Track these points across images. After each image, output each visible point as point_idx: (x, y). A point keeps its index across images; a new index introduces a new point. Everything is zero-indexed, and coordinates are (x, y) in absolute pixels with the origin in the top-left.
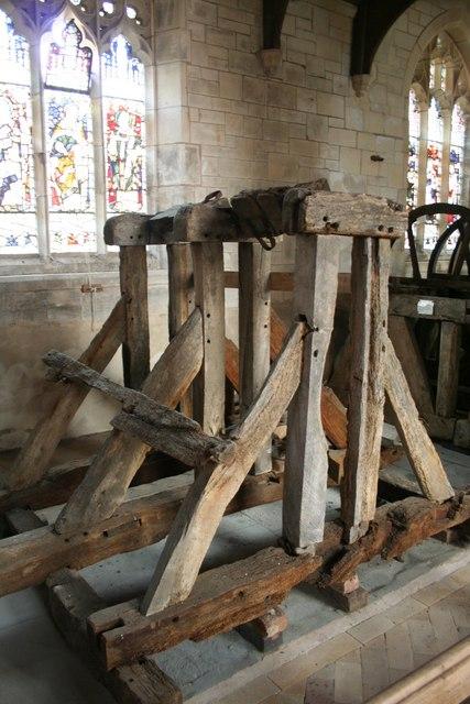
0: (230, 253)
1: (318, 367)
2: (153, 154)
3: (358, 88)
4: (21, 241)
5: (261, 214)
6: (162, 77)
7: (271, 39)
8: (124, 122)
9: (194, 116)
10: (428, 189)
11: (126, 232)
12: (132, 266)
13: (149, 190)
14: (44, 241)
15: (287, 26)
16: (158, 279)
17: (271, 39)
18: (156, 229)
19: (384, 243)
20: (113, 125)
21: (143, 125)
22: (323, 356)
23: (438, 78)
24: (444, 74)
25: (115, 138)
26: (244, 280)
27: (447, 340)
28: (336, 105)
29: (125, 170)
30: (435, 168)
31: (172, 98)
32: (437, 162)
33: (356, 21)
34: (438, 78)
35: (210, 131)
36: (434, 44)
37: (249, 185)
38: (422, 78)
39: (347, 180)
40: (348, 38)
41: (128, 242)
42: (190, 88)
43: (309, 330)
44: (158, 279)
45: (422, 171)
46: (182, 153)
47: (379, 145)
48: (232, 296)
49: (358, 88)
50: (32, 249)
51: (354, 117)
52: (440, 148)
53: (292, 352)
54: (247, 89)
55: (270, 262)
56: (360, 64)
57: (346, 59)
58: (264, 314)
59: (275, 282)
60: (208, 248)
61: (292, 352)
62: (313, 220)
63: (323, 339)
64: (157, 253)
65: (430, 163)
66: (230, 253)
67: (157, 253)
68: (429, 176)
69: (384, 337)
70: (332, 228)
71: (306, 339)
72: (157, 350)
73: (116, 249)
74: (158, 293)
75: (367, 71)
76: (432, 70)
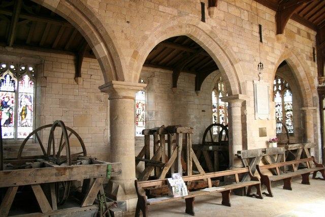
0: (166, 136)
1: (180, 153)
2: (147, 113)
3: (197, 94)
4: (9, 135)
5: (170, 130)
6: (149, 96)
7: (175, 85)
8: (140, 105)
9: (157, 104)
10: (221, 117)
11: (146, 133)
12: (147, 139)
13: (146, 121)
14: (16, 134)
15: (179, 81)
16: (152, 143)
17: (175, 85)
18: (152, 132)
19: (190, 135)
20: (138, 106)
21: (144, 106)
22: (181, 152)
23: (221, 87)
24: (223, 86)
25: (138, 109)
26: (168, 141)
27: (216, 155)
28: (192, 99)
29: (140, 117)
30: (223, 111)
31: (152, 100)
32: (223, 110)
33: (196, 78)
34: (221, 87)
35: (160, 107)
36: (219, 80)
37: (170, 124)
38: (216, 88)
39: (196, 117)
40: (194, 82)
41: (146, 134)
42: (156, 98)
43: (178, 147)
44: (152, 143)
45: (218, 112)
46: (154, 112)
47: (204, 107)
48: (167, 144)
49: (197, 94)
50: (12, 137)
51: (197, 101)
52: (224, 106)
53: (176, 151)
54: (169, 97)
55: (173, 138)
56: (198, 88)
57: (194, 87)
58: (172, 147)
59: (174, 141)
60: (162, 136)
61: (176, 151)
62: (178, 131)
63: (181, 149)
64: (152, 137)
65: (221, 110)
66: (166, 136)
67: (152, 137)
68: (220, 114)
69: (191, 149)
70: (181, 132)
71: (178, 149)
72: (152, 155)
73: (144, 136)
74: (152, 146)
75: (199, 90)
76: (219, 85)
